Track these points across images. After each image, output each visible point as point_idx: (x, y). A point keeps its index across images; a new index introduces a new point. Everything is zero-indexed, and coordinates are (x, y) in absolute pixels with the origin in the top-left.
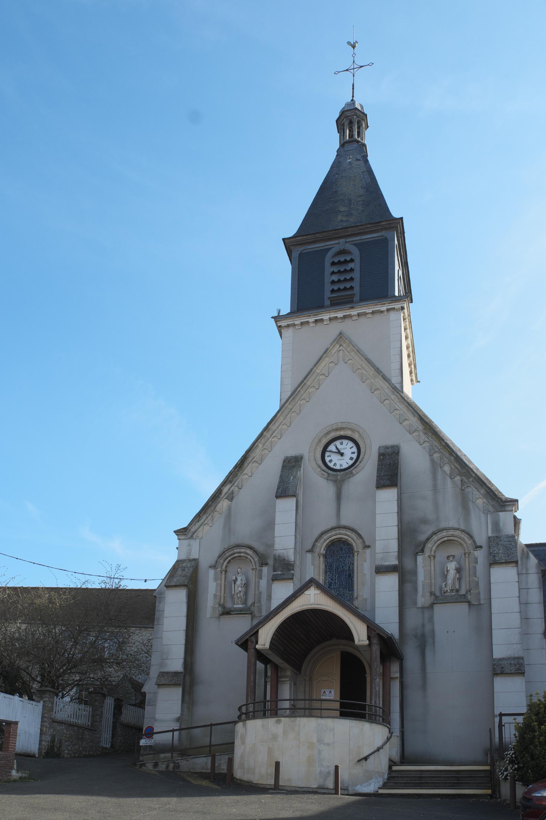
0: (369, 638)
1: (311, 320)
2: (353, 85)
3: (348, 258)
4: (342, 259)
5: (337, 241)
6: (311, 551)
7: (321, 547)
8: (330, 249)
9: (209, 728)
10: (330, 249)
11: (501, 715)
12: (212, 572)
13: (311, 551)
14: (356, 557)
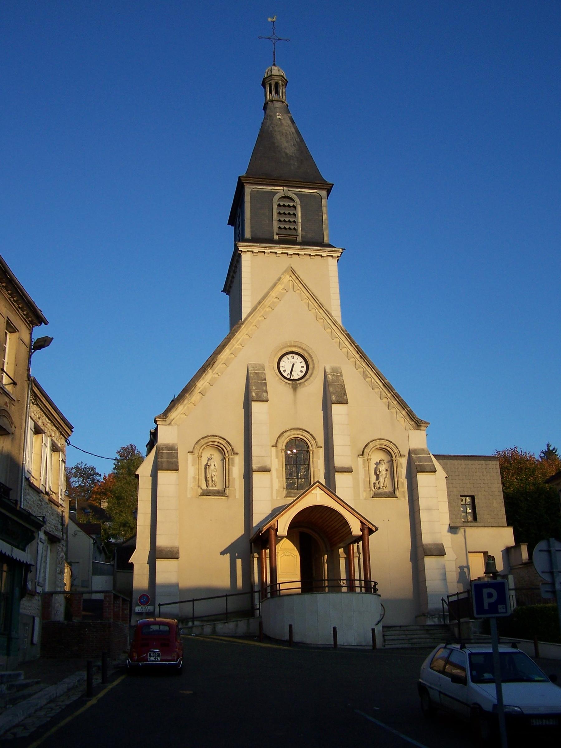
0: (362, 530)
1: (267, 251)
2: (274, 52)
3: (291, 204)
4: (286, 204)
5: (282, 188)
6: (275, 446)
7: (282, 444)
8: (277, 193)
9: (225, 598)
10: (277, 193)
11: (160, 605)
12: (190, 457)
13: (275, 446)
14: (311, 455)
